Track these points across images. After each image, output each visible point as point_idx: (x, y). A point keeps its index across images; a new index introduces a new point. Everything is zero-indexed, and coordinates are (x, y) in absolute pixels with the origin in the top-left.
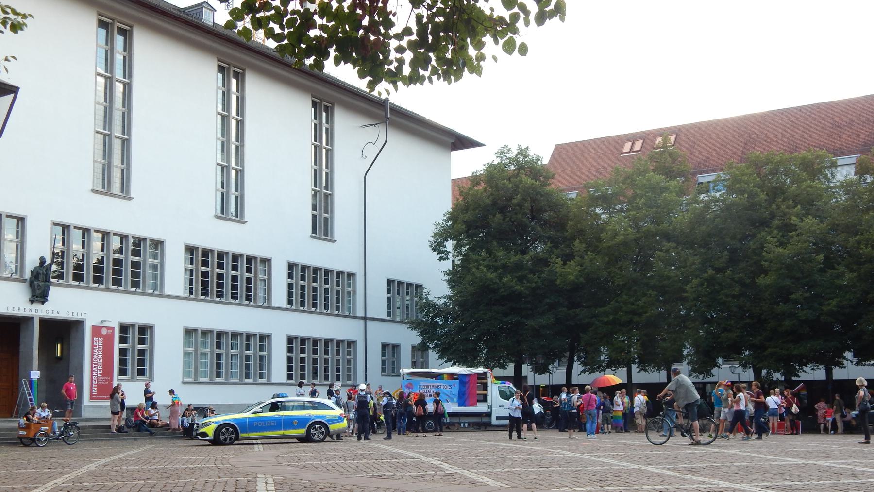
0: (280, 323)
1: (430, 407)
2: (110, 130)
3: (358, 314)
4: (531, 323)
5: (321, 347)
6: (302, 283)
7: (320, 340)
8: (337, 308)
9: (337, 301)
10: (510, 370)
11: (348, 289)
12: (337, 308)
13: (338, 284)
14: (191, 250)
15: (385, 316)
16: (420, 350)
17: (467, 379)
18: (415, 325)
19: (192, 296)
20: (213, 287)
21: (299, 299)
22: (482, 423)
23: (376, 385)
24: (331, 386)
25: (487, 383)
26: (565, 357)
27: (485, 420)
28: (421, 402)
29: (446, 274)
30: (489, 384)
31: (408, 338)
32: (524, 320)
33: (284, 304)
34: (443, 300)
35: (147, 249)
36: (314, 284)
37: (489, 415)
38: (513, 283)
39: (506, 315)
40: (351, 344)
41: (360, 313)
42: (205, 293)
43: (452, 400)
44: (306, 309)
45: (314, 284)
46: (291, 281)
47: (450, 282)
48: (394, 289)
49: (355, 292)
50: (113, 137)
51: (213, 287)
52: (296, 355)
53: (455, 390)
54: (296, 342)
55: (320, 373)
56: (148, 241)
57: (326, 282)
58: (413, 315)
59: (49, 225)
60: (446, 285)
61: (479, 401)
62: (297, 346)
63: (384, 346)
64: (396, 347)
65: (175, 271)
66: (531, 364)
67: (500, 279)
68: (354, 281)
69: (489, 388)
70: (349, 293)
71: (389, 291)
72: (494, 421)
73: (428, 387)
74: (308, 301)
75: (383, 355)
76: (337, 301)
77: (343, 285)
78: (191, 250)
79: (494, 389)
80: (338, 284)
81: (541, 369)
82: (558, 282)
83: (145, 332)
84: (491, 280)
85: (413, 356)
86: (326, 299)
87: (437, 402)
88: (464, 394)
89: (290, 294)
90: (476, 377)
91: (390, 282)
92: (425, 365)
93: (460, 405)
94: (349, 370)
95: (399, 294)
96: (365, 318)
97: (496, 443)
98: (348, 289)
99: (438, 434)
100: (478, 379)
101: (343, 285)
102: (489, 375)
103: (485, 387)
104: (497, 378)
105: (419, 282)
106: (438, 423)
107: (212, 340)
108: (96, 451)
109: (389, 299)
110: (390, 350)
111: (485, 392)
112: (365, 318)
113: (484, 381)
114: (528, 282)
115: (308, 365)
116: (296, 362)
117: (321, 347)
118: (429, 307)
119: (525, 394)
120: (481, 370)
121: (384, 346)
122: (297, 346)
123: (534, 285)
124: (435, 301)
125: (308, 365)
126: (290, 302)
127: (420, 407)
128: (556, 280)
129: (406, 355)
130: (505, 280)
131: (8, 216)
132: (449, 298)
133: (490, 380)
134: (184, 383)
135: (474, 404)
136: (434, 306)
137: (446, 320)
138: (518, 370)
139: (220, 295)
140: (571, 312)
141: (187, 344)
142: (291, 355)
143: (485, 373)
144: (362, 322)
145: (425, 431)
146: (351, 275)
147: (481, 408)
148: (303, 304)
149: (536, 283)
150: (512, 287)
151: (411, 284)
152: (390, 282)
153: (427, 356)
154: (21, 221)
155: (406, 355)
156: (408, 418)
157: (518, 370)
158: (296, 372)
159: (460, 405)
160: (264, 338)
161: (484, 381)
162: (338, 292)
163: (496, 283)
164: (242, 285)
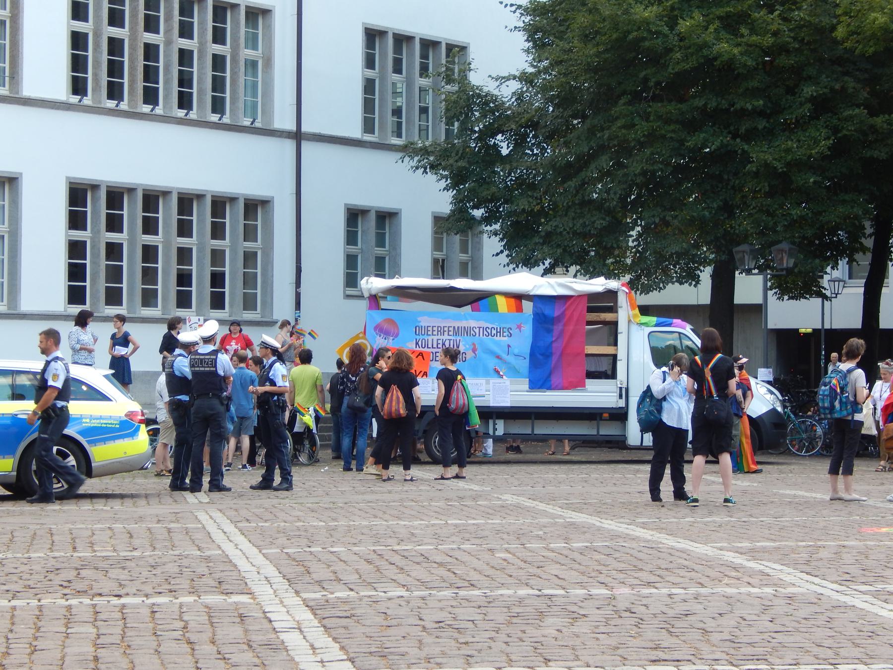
1: (428, 392)
4: (762, 154)
5: (168, 214)
6: (218, 49)
7: (200, 197)
8: (218, 106)
9: (218, 84)
10: (700, 293)
11: (249, 53)
12: (218, 106)
13: (219, 37)
15: (355, 131)
16: (454, 226)
17: (554, 311)
18: (434, 159)
20: (132, 78)
21: (209, 94)
22: (594, 437)
23: (318, 322)
24: (174, 324)
25: (615, 324)
26: (864, 249)
27: (608, 430)
28: (402, 377)
29: (527, 11)
30: (622, 327)
31: (421, 197)
32: (741, 145)
33: (61, 90)
34: (515, 86)
36: (150, 38)
38: (708, 36)
39: (692, 126)
40: (255, 207)
41: (284, 121)
43: (514, 372)
44: (226, 120)
45: (150, 38)
46: (80, 26)
47: (532, 31)
48: (383, 55)
49: (268, 61)
51: (132, 78)
52: (95, 235)
53: (523, 340)
54: (132, 202)
55: (131, 282)
56: (390, 36)
57: (186, 31)
58: (437, 133)
60: (520, 40)
61: (591, 375)
62: (96, 210)
63: (354, 215)
64: (386, 218)
66: (762, 269)
67: (672, 23)
68: (269, 28)
69: (622, 339)
70: (252, 65)
71: (370, 62)
73: (441, 331)
74: (132, 82)
75: (351, 238)
76: (218, 84)
77: (168, 31)
79: (636, 341)
80: (219, 37)
81: (799, 284)
82: (840, 32)
84: (647, 22)
85: (437, 244)
86: (185, 80)
87: (448, 379)
88: (547, 355)
89: (78, 63)
90: (585, 304)
91: (372, 36)
92: (471, 269)
93: (535, 385)
94: (249, 281)
95: (398, 70)
96: (298, 136)
97: (601, 504)
98: (249, 53)
99: (454, 470)
100: (591, 310)
101: (235, 39)
102: (622, 299)
103: (612, 331)
104: (645, 310)
105: (444, 31)
106: (447, 437)
108: (794, 461)
109: (369, 86)
110: (370, 231)
111: (609, 350)
112: (298, 136)
113: (608, 316)
114: (753, 31)
115: (131, 265)
116: (95, 255)
117: (132, 212)
118: (466, 104)
119: (706, 362)
120: (599, 284)
121: (354, 215)
122: (96, 210)
123: (769, 40)
124: (491, 87)
125: (131, 265)
126: (78, 87)
127: (396, 393)
128: (833, 28)
129: (416, 240)
130: (684, 25)
132: (525, 78)
133: (624, 313)
135: (577, 385)
136: (487, 103)
137: (520, 143)
138: (723, 286)
140: (879, 121)
142: (78, 235)
143: (611, 295)
144: (289, 146)
145: (787, 452)
147: (598, 394)
148: (115, 92)
149: (775, 34)
150: (706, 45)
151: (435, 44)
152: (372, 36)
153: (478, 247)
155: (416, 240)
156: (391, 423)
157: (723, 286)
158: (95, 284)
159: (535, 385)
161: (608, 316)
162: (218, 62)
163: (658, 33)
164: (202, 75)
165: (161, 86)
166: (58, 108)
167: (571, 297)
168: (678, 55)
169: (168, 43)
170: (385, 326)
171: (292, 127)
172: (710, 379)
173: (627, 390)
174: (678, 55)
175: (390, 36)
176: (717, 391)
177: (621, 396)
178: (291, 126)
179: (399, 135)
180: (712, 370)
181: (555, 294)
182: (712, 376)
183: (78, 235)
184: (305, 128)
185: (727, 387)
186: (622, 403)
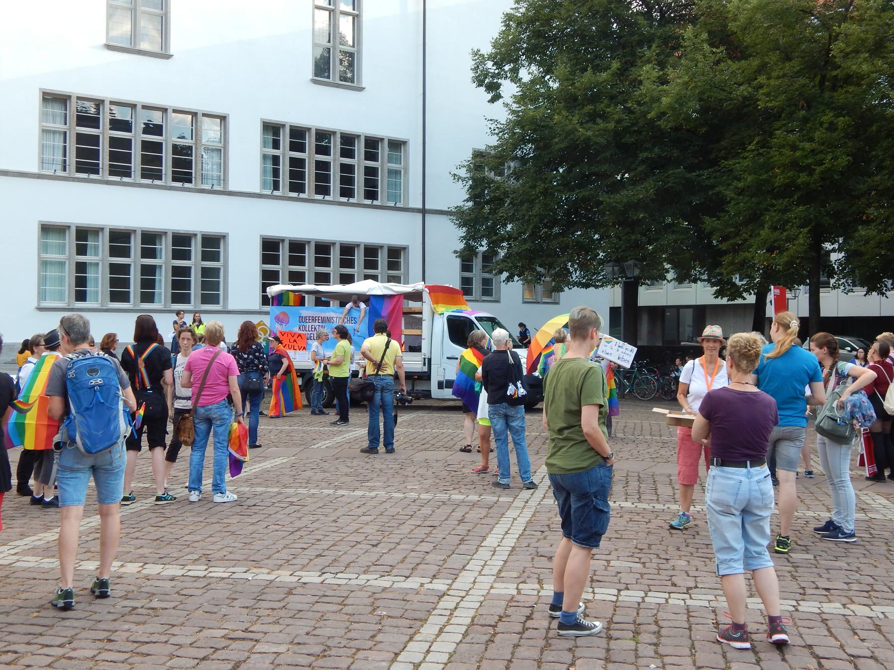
0: (243, 216)
2: (335, 5)
3: (412, 205)
14: (272, 129)
19: (276, 193)
30: (426, 315)
35: (383, 151)
37: (425, 377)
42: (347, 192)
50: (338, 12)
59: (36, 100)
65: (246, 162)
69: (425, 325)
72: (435, 392)
78: (272, 129)
83: (213, 244)
96: (424, 211)
107: (71, 240)
112: (424, 211)
126: (276, 186)
131: (204, 115)
134: (40, 309)
139: (347, 192)
141: (44, 247)
144: (419, 216)
146: (397, 145)
154: (223, 119)
160: (213, 244)
165: (332, 185)
166: (253, 197)
167: (394, 296)
168: (557, 140)
169: (335, 160)
170: (281, 316)
171: (420, 206)
172: (143, 370)
173: (430, 360)
174: (557, 140)
175: (338, 136)
176: (151, 383)
177: (424, 364)
178: (419, 206)
179: (65, 170)
180: (146, 361)
181: (381, 294)
182: (145, 367)
183: (467, 274)
184: (426, 207)
185: (161, 376)
186: (425, 369)
